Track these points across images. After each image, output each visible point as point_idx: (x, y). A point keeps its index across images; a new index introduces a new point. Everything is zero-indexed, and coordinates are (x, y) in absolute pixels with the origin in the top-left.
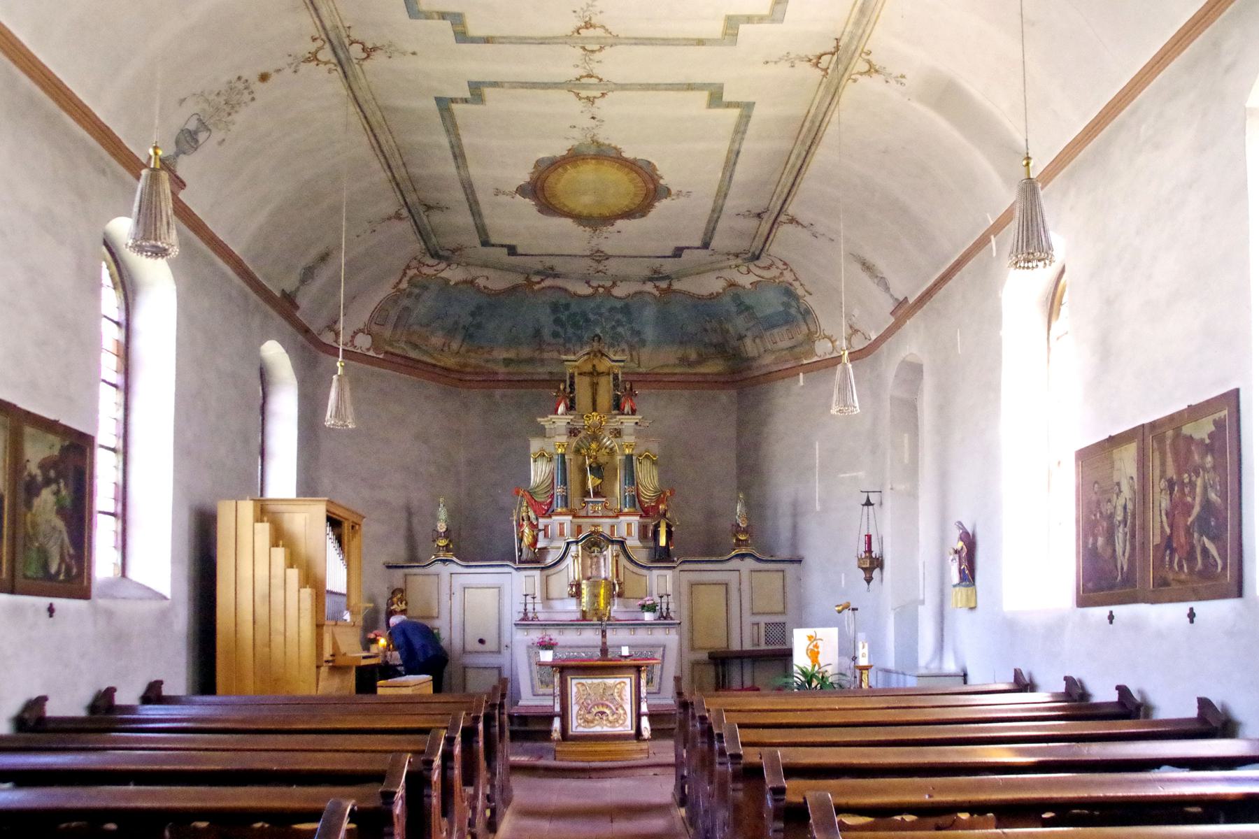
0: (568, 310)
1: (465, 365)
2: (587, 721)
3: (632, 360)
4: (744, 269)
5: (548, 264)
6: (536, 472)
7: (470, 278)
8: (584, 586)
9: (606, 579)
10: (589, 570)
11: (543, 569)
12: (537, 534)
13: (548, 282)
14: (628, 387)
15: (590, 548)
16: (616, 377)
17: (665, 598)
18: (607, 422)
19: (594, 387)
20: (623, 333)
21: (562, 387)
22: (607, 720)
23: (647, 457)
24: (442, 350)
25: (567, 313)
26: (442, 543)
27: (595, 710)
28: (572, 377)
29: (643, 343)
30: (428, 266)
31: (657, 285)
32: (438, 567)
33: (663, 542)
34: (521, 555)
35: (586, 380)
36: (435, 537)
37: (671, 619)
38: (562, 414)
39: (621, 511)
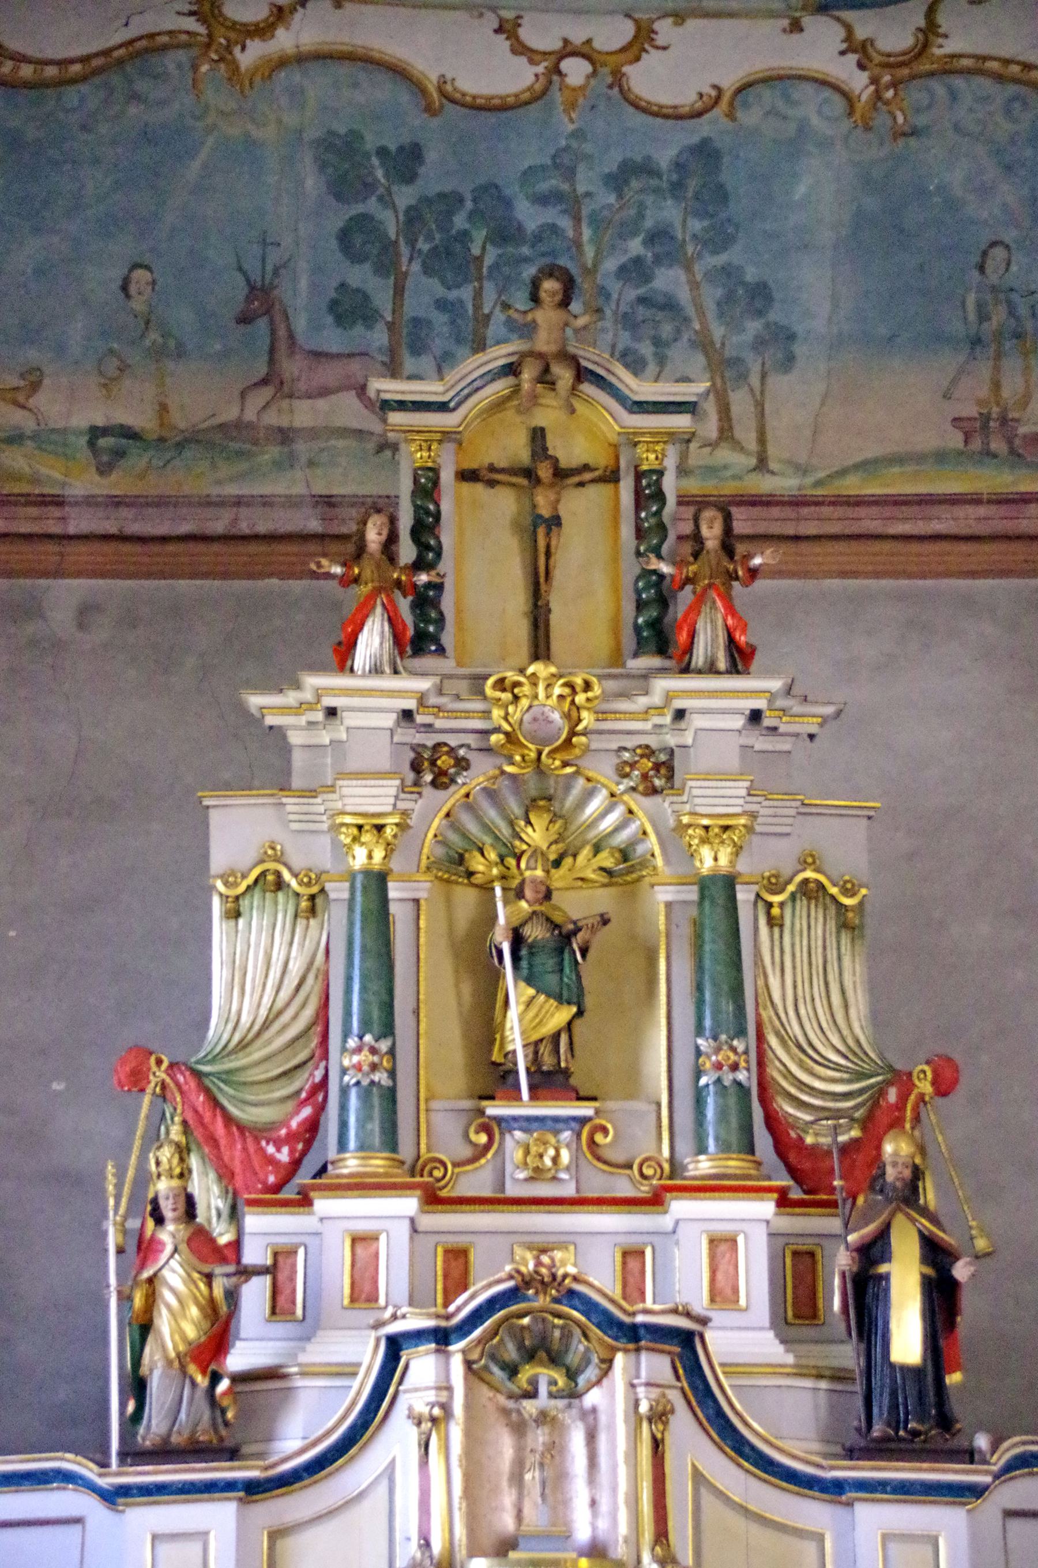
0: (410, 178)
3: (726, 433)
6: (238, 971)
10: (508, 1499)
11: (253, 1489)
12: (232, 1296)
14: (711, 533)
15: (512, 1371)
18: (602, 715)
21: (374, 536)
23: (812, 892)
25: (405, 197)
31: (861, 33)
34: (137, 1417)
38: (376, 670)
39: (676, 1167)
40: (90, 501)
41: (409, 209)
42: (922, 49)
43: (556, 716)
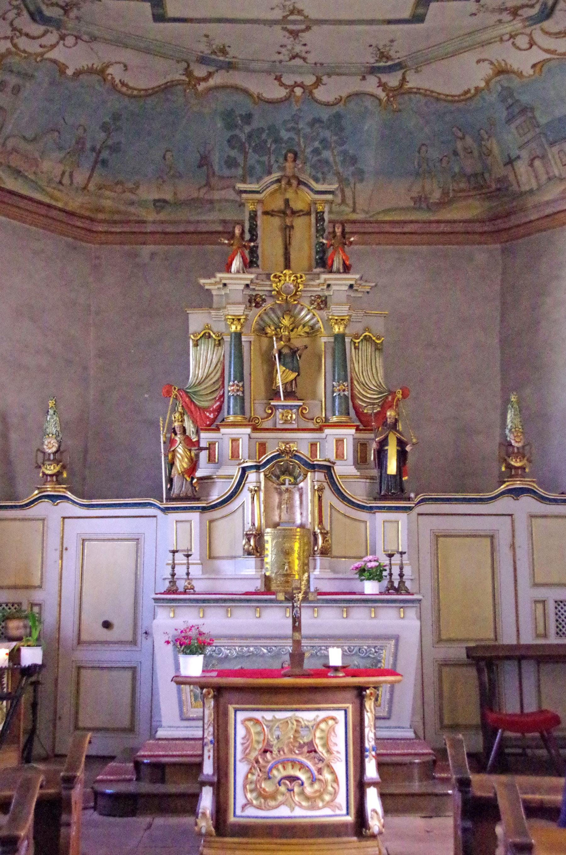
0: (249, 123)
1: (100, 210)
2: (262, 795)
4: (522, 41)
5: (218, 42)
7: (98, 65)
8: (267, 538)
9: (302, 526)
10: (277, 512)
11: (204, 509)
12: (197, 456)
13: (216, 80)
15: (278, 477)
16: (320, 218)
17: (397, 558)
18: (306, 286)
19: (287, 230)
20: (331, 159)
21: (237, 231)
22: (302, 793)
24: (60, 183)
25: (247, 129)
26: (51, 469)
27: (277, 774)
28: (253, 217)
29: (360, 175)
30: (27, 35)
31: (384, 80)
32: (43, 508)
33: (392, 468)
34: (170, 489)
35: (276, 221)
36: (40, 461)
37: (408, 593)
38: (238, 272)
39: (326, 419)
40: (154, 222)
41: (249, 133)
42: (401, 86)
43: (292, 286)
